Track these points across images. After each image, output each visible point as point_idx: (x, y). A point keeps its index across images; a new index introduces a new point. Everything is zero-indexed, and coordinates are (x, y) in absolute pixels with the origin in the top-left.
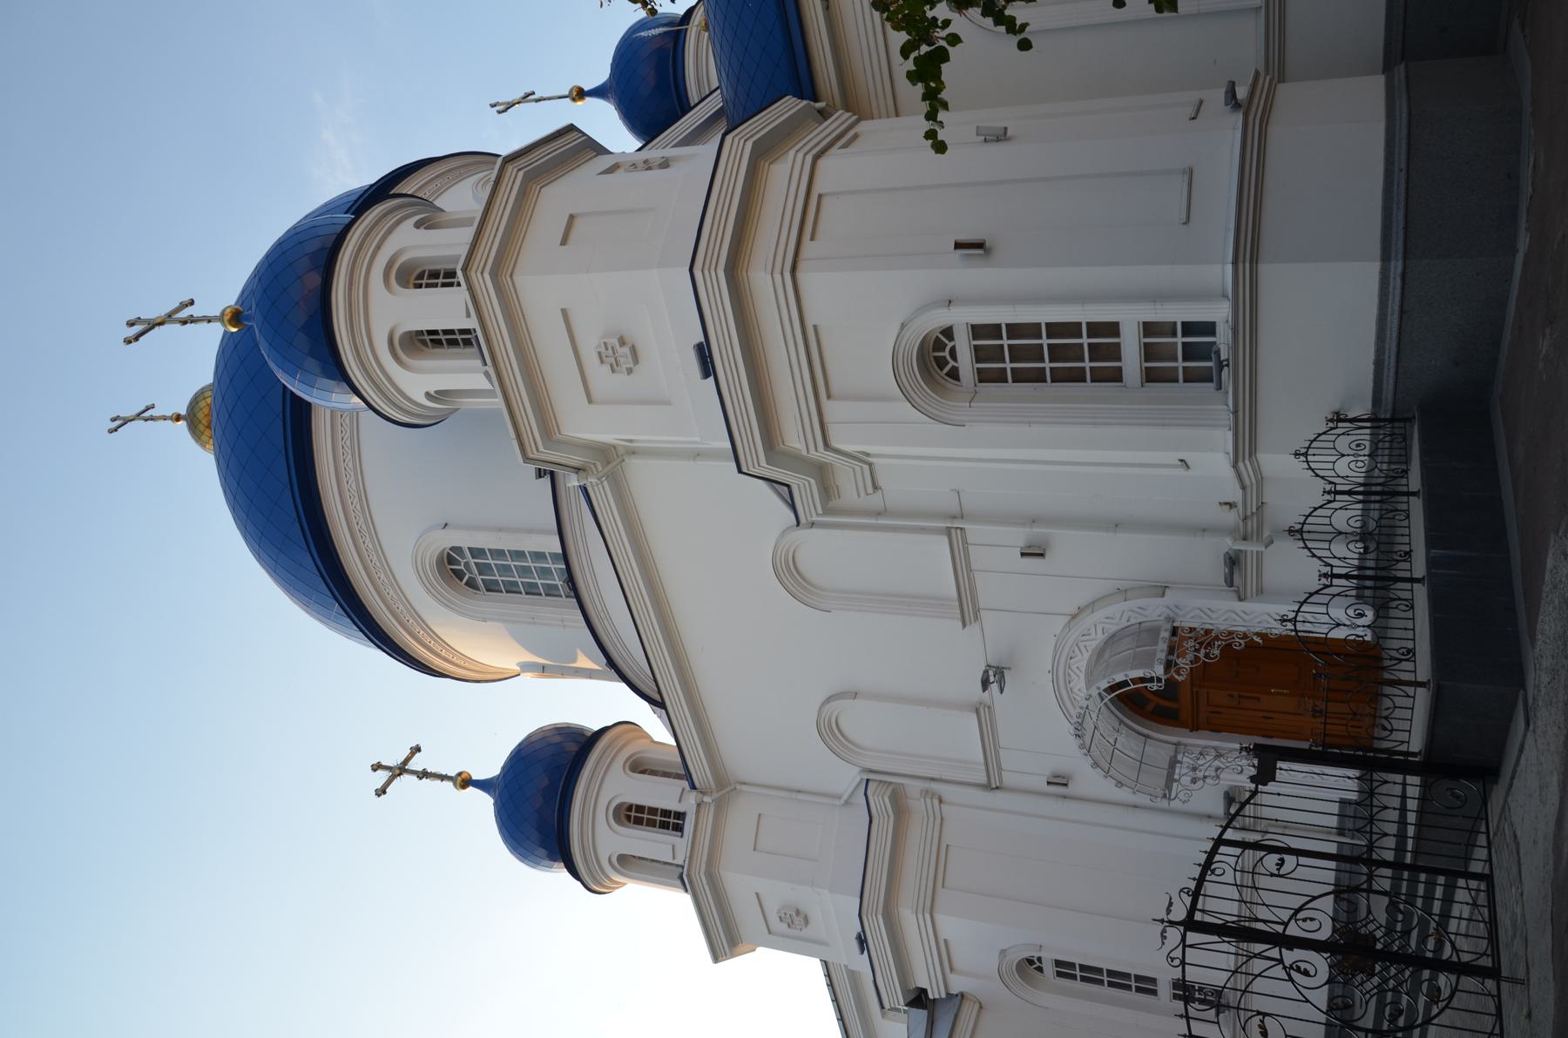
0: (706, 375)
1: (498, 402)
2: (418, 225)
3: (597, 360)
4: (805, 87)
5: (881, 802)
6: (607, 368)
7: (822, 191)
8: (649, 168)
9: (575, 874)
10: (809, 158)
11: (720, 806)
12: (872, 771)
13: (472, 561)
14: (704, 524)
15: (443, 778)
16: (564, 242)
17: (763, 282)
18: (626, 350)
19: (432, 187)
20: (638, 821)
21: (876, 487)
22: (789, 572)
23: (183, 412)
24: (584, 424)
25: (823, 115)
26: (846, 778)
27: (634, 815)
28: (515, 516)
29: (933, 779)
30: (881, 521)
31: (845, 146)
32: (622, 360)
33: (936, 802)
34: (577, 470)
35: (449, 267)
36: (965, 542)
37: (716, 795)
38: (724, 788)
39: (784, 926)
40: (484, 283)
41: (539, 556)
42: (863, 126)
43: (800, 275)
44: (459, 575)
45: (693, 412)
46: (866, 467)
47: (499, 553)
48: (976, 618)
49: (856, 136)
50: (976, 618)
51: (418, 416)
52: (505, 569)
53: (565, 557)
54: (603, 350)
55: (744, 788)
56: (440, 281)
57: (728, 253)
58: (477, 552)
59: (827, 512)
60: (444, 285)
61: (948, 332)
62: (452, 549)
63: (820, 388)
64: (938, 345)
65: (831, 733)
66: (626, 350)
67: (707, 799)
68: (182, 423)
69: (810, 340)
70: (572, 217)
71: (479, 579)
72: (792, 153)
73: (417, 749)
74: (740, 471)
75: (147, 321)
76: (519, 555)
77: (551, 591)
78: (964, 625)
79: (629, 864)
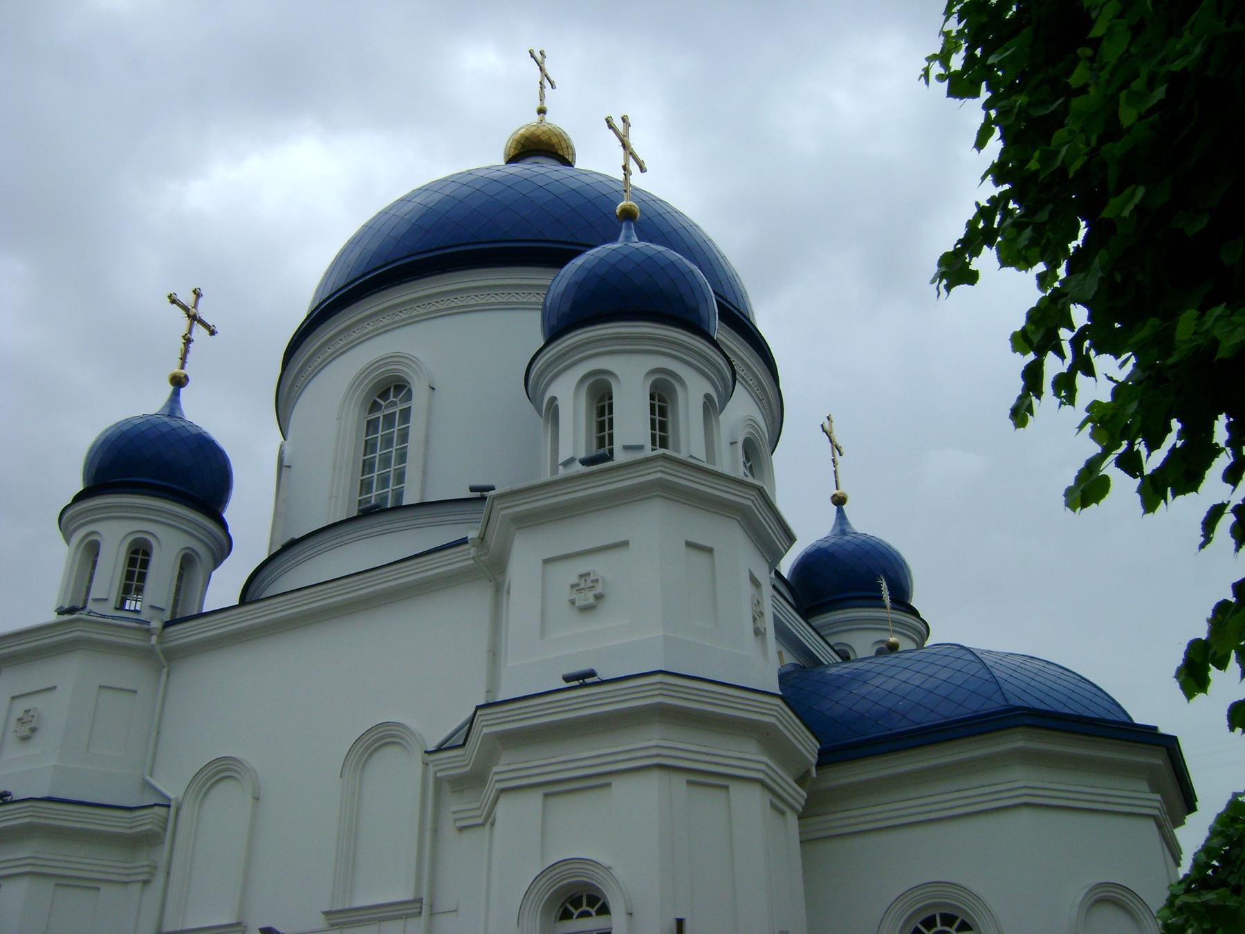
0: (567, 679)
1: (547, 477)
2: (707, 396)
3: (584, 570)
4: (830, 756)
5: (147, 822)
6: (575, 580)
7: (731, 789)
8: (755, 619)
9: (79, 498)
10: (760, 776)
11: (146, 654)
12: (178, 809)
13: (397, 410)
14: (427, 665)
15: (184, 359)
16: (689, 544)
17: (651, 741)
18: (591, 600)
19: (749, 378)
20: (132, 562)
21: (462, 829)
22: (382, 738)
23: (548, 118)
24: (525, 557)
25: (801, 780)
26: (172, 789)
27: (139, 557)
28: (442, 460)
29: (168, 874)
30: (428, 835)
31: (773, 805)
32: (582, 595)
33: (145, 877)
34: (482, 538)
35: (670, 442)
36: (408, 916)
37: (158, 648)
38: (164, 659)
39: (20, 714)
40: (653, 474)
41: (400, 477)
42: (792, 819)
43: (655, 776)
44: (384, 395)
45: (533, 666)
46: (480, 821)
47: (404, 437)
48: (332, 925)
49: (783, 813)
50: (332, 925)
51: (537, 384)
52: (388, 442)
53: (398, 508)
54: (592, 577)
55: (164, 676)
56: (657, 418)
57: (680, 709)
58: (406, 415)
59: (438, 781)
60: (653, 421)
61: (604, 910)
62: (410, 391)
63: (554, 789)
64: (593, 900)
65: (221, 771)
66: (591, 600)
67: (154, 639)
68: (536, 118)
69: (597, 781)
70: (709, 551)
71: (380, 415)
72: (765, 759)
73: (213, 333)
74: (478, 708)
75: (627, 135)
76: (402, 457)
77: (366, 486)
78: (326, 913)
79: (92, 550)
